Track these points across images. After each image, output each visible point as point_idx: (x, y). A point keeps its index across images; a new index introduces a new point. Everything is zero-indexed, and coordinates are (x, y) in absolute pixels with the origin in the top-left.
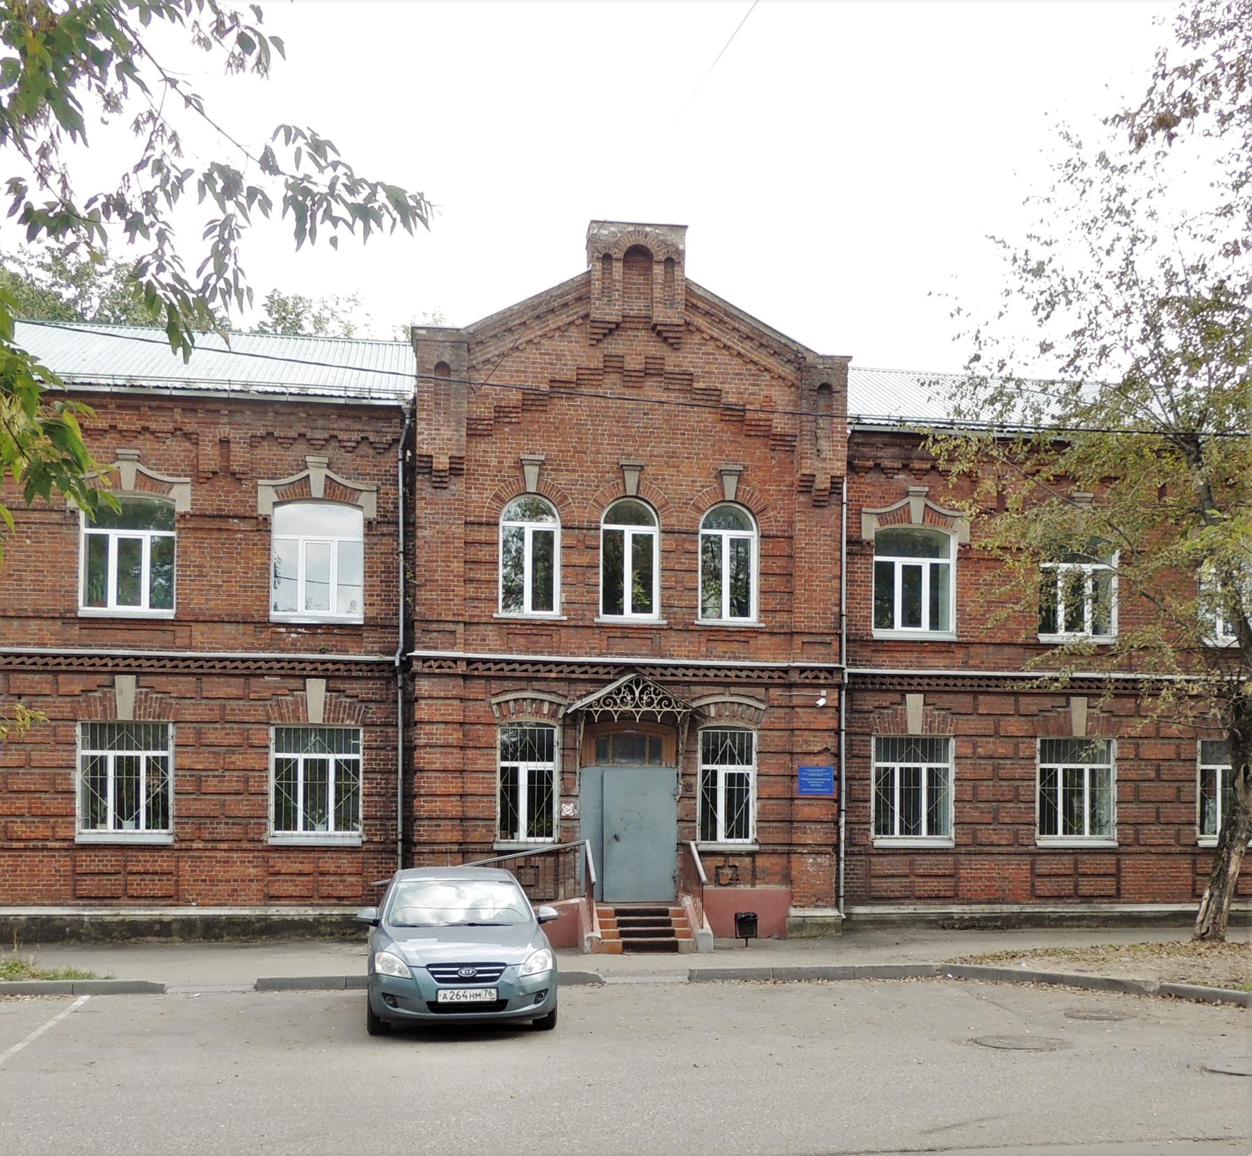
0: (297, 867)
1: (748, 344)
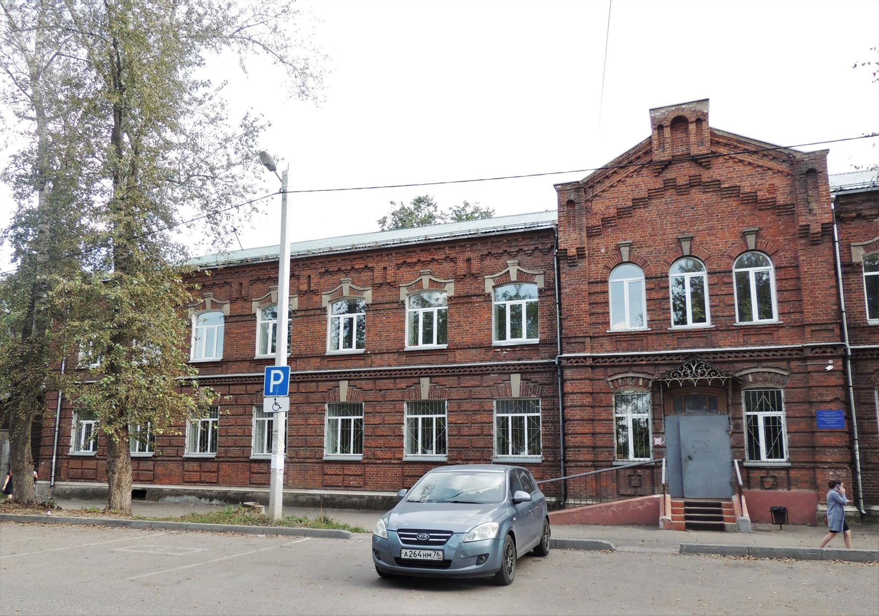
1: (755, 157)
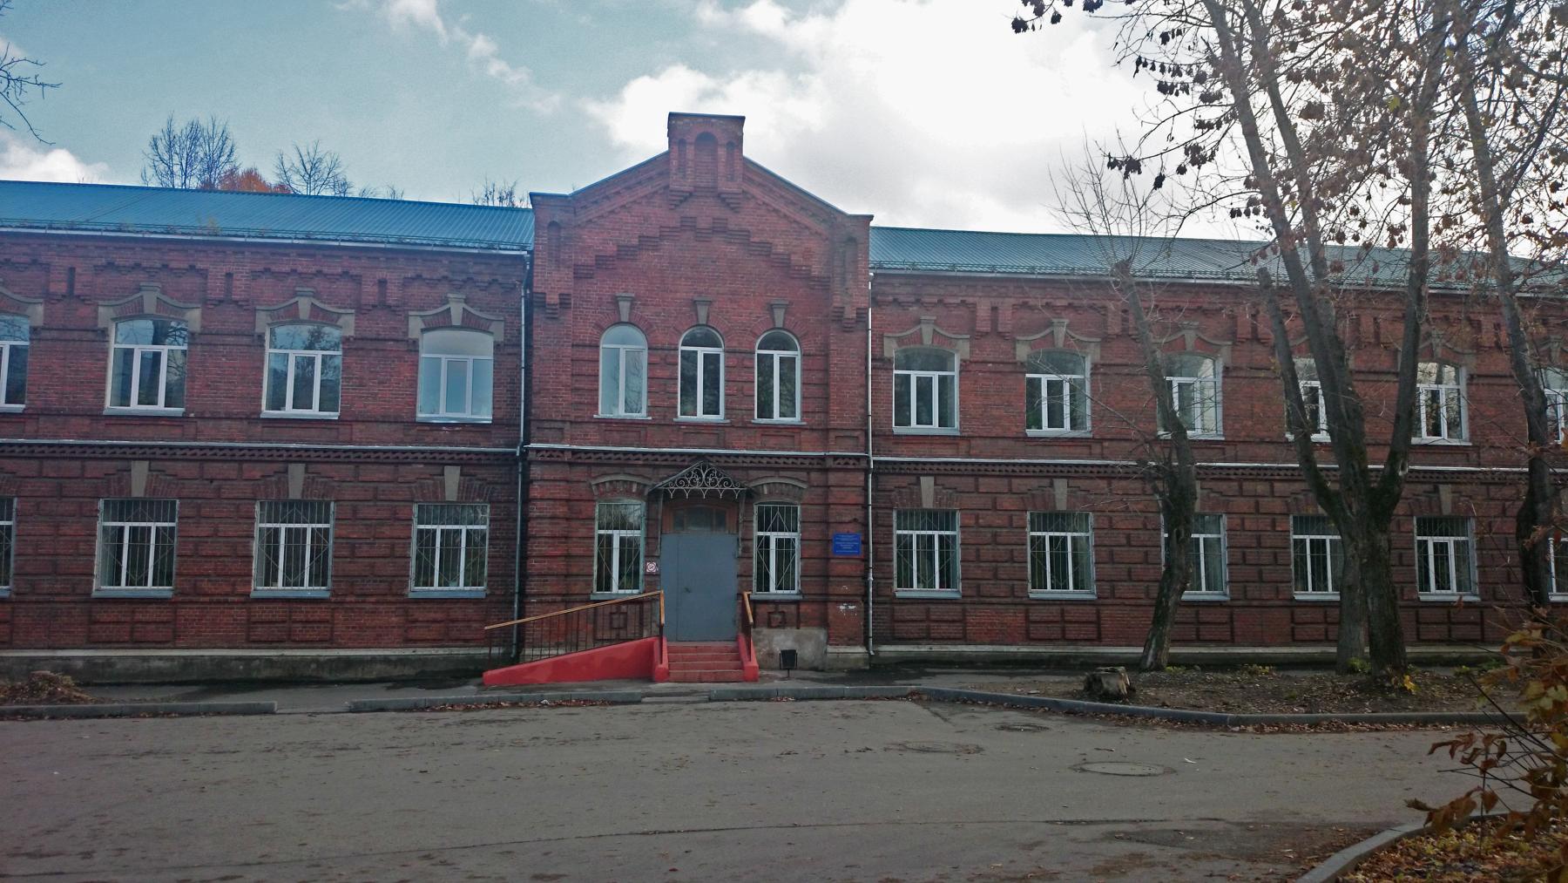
0: (432, 615)
